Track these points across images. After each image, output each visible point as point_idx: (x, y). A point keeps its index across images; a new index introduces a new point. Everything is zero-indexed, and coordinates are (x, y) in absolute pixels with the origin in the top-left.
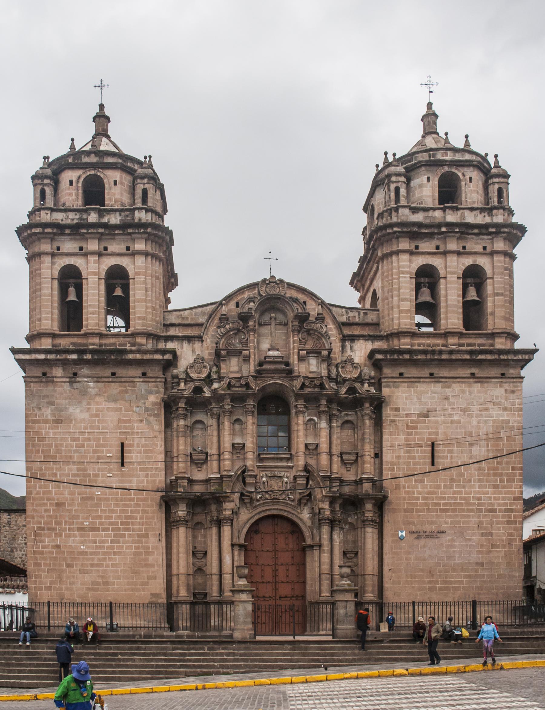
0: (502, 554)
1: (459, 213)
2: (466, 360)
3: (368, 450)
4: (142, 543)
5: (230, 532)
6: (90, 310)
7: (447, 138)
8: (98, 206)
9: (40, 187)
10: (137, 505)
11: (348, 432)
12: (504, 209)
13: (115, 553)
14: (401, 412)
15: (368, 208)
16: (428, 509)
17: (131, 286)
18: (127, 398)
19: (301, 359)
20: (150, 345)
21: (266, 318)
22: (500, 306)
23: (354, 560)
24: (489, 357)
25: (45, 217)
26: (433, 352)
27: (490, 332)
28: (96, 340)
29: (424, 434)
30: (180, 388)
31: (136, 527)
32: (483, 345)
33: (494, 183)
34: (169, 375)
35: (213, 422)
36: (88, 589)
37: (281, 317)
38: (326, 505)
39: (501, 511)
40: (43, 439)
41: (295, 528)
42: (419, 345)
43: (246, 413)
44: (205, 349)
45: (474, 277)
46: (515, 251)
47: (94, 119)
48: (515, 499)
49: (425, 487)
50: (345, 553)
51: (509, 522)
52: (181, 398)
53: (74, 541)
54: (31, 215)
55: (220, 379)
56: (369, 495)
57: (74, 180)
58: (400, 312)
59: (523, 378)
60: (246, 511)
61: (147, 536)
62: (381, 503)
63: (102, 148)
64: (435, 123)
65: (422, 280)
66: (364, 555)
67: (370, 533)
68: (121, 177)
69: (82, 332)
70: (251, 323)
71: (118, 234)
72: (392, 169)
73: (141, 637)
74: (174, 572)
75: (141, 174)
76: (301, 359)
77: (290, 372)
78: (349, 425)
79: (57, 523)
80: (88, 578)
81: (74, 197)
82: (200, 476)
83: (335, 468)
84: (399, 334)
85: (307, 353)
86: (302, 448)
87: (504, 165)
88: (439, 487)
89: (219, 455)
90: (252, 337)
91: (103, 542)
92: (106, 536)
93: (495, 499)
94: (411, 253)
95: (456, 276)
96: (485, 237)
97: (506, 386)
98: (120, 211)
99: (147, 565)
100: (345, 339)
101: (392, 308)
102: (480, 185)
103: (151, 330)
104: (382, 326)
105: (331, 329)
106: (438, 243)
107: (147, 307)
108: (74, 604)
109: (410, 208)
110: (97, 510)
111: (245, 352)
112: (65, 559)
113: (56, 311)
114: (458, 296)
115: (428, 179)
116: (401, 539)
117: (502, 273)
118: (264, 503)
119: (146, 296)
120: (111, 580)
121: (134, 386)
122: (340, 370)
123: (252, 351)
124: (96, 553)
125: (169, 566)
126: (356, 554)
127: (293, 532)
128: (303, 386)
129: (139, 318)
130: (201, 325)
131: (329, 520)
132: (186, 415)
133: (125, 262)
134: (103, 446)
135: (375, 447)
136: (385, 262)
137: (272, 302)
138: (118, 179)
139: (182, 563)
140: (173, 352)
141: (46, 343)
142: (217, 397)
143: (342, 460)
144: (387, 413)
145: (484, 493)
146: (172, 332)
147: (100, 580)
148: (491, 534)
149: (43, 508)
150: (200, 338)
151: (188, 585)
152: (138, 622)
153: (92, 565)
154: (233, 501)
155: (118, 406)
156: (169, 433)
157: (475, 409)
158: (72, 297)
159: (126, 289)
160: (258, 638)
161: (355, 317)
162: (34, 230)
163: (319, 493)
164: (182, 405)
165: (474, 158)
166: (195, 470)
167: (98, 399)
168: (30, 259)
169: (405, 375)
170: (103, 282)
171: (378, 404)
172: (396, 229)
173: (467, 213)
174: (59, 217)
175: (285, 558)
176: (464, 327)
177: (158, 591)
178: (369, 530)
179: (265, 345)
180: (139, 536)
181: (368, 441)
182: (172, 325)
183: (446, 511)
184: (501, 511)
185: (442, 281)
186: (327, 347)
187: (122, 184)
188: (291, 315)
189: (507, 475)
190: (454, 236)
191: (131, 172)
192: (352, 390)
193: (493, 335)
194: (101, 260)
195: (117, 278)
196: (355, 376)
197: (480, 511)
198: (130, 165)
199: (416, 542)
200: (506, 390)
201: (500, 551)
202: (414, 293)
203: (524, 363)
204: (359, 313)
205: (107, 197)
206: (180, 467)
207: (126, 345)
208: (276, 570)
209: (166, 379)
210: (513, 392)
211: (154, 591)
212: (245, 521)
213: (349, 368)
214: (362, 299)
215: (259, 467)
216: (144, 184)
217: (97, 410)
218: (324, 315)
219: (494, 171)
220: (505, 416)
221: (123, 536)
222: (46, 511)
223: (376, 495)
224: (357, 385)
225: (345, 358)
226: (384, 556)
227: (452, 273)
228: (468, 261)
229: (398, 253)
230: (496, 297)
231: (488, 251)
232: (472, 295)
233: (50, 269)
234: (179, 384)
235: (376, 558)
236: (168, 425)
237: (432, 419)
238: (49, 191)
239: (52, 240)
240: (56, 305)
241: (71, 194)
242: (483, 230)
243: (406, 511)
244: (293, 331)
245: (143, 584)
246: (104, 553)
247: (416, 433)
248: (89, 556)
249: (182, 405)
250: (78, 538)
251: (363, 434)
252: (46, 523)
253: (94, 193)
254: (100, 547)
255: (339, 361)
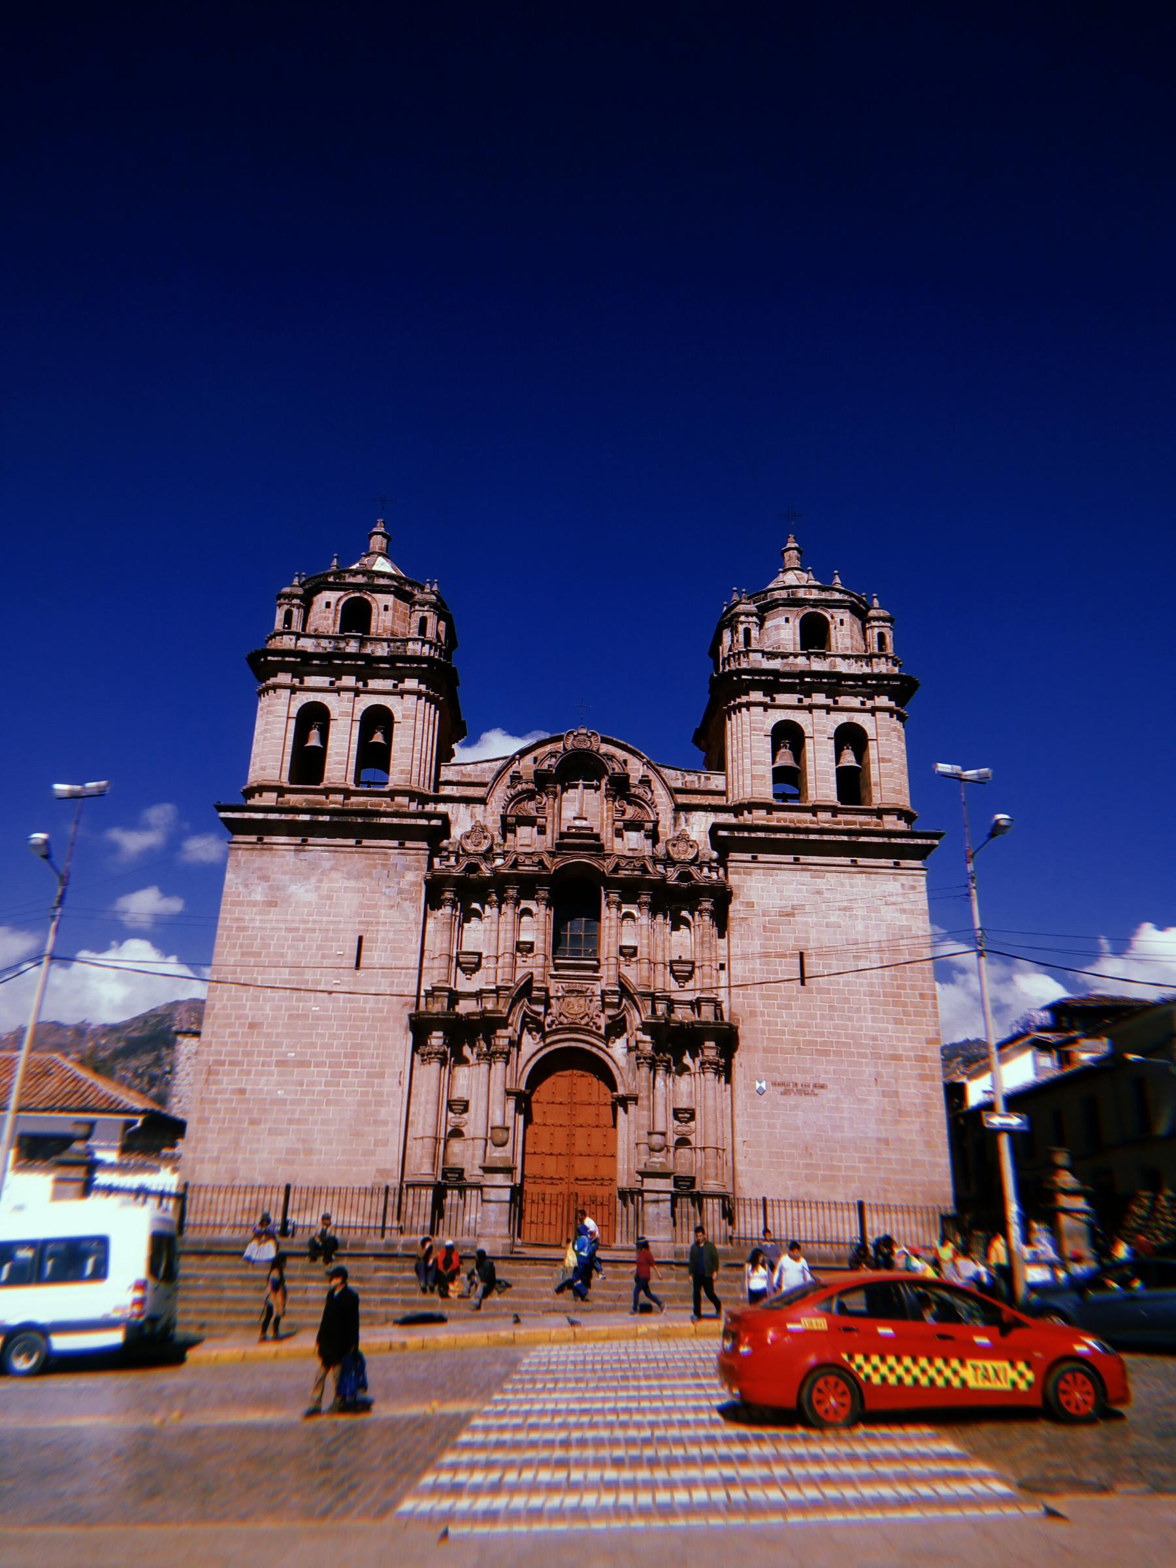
0: (916, 1127)
1: (828, 660)
10: (373, 1027)
13: (329, 1103)
20: (413, 807)
29: (789, 940)
31: (367, 1061)
32: (868, 824)
36: (278, 1161)
40: (245, 929)
44: (490, 816)
48: (929, 1042)
53: (267, 1083)
55: (504, 854)
61: (382, 1075)
63: (375, 568)
76: (619, 834)
77: (601, 848)
79: (246, 1054)
80: (281, 1143)
81: (331, 622)
84: (751, 806)
88: (813, 1017)
91: (313, 1084)
97: (903, 879)
99: (376, 1122)
100: (679, 808)
103: (415, 786)
105: (660, 796)
108: (251, 1188)
109: (764, 653)
115: (787, 620)
116: (761, 1092)
117: (888, 734)
120: (318, 1146)
124: (300, 1102)
128: (617, 868)
130: (484, 785)
134: (333, 940)
138: (390, 604)
140: (444, 817)
145: (880, 1030)
146: (446, 791)
149: (228, 1030)
150: (483, 801)
153: (290, 1121)
155: (360, 885)
158: (314, 741)
159: (388, 737)
163: (635, 1019)
167: (334, 875)
171: (722, 897)
173: (838, 660)
174: (308, 645)
177: (388, 1166)
183: (826, 1053)
189: (914, 1005)
192: (685, 876)
193: (880, 813)
195: (377, 721)
199: (782, 1100)
200: (903, 885)
202: (770, 755)
207: (381, 805)
208: (571, 1136)
215: (552, 977)
217: (330, 890)
220: (903, 920)
221: (345, 1075)
224: (693, 869)
225: (677, 834)
232: (849, 759)
237: (798, 918)
241: (326, 618)
246: (312, 1102)
247: (777, 938)
248: (288, 1107)
252: (230, 1054)
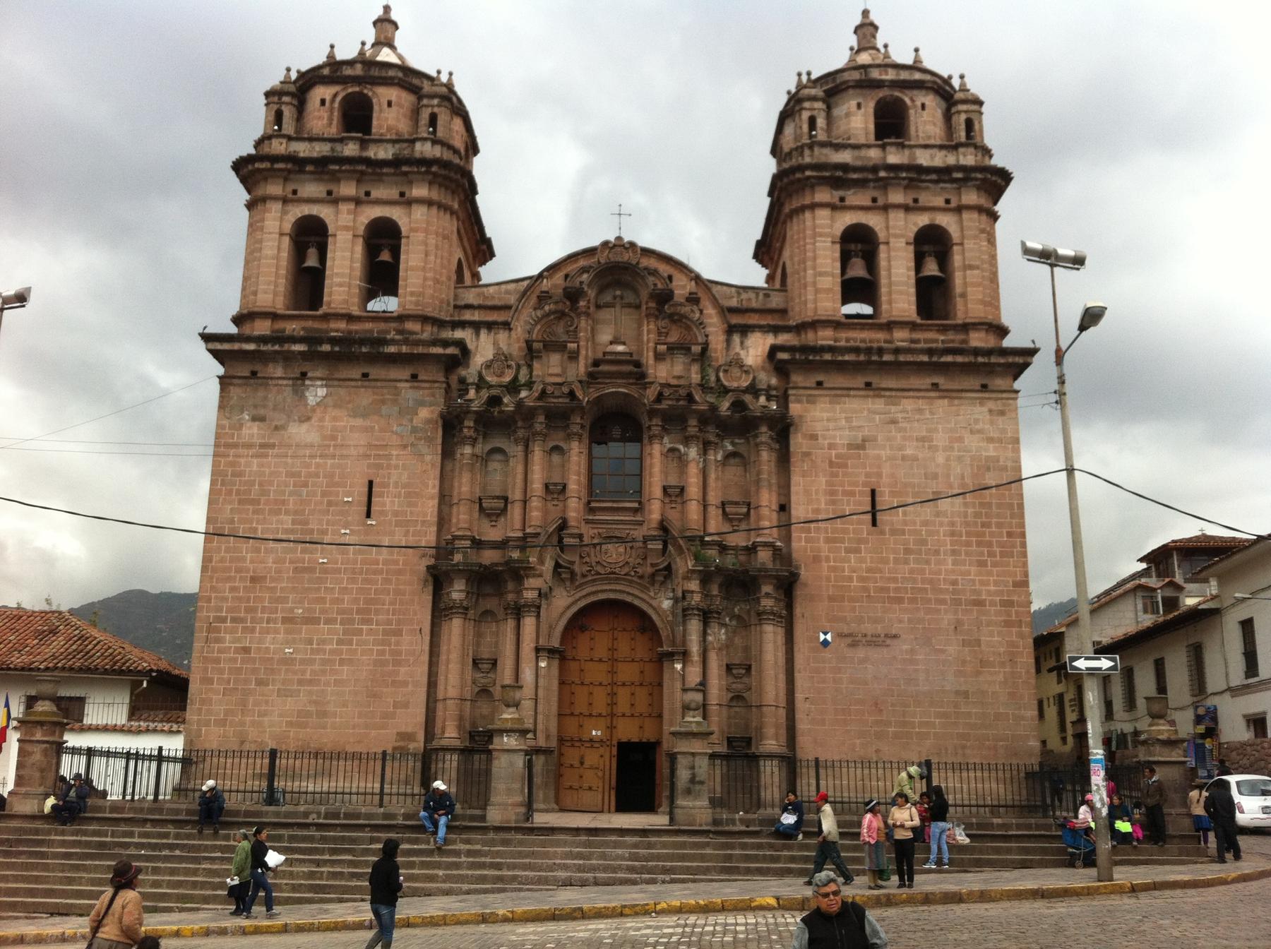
1: (907, 152)
2: (922, 364)
3: (767, 499)
4: (390, 645)
5: (534, 627)
6: (336, 280)
7: (886, 51)
8: (360, 135)
9: (276, 107)
10: (387, 581)
11: (733, 472)
12: (976, 147)
13: (342, 662)
14: (820, 440)
15: (776, 150)
16: (869, 596)
17: (403, 248)
18: (383, 412)
19: (659, 357)
21: (607, 298)
22: (974, 285)
23: (745, 680)
24: (959, 359)
25: (278, 147)
26: (869, 351)
27: (960, 322)
28: (342, 325)
30: (467, 397)
33: (959, 112)
34: (454, 379)
35: (518, 450)
36: (290, 724)
37: (630, 297)
38: (694, 585)
39: (993, 603)
40: (240, 474)
41: (644, 623)
42: (848, 340)
43: (569, 437)
44: (511, 342)
45: (932, 244)
46: (996, 208)
47: (375, 23)
49: (862, 560)
50: (729, 668)
51: (1008, 624)
52: (469, 412)
53: (274, 641)
54: (259, 143)
55: (529, 385)
56: (766, 570)
57: (328, 98)
58: (817, 291)
59: (1017, 392)
60: (565, 593)
61: (398, 633)
62: (788, 585)
64: (874, 37)
65: (853, 247)
66: (760, 672)
67: (771, 635)
68: (399, 97)
69: (320, 312)
70: (582, 303)
71: (387, 174)
72: (806, 92)
73: (319, 818)
74: (440, 695)
75: (438, 100)
76: (659, 357)
77: (643, 376)
78: (737, 460)
79: (248, 610)
80: (290, 704)
81: (325, 121)
82: (493, 533)
83: (712, 528)
84: (814, 325)
85: (668, 349)
86: (658, 492)
87: (975, 88)
89: (525, 502)
90: (583, 324)
91: (323, 642)
92: (330, 632)
93: (982, 583)
94: (833, 207)
95: (903, 240)
96: (948, 185)
97: (991, 405)
98: (394, 142)
100: (731, 330)
101: (805, 286)
102: (939, 114)
103: (429, 311)
104: (791, 313)
105: (710, 316)
106: (875, 194)
107: (425, 279)
110: (319, 589)
111: (572, 346)
112: (254, 671)
113: (282, 281)
114: (908, 269)
115: (859, 106)
117: (975, 237)
118: (594, 580)
119: (426, 263)
120: (331, 708)
121: (398, 395)
122: (721, 374)
123: (582, 343)
125: (432, 684)
126: (749, 668)
127: (643, 630)
128: (660, 398)
129: (412, 294)
130: (508, 307)
131: (698, 609)
132: (476, 439)
133: (395, 213)
134: (337, 485)
135: (779, 494)
136: (795, 220)
137: (618, 274)
138: (394, 99)
139: (454, 680)
140: (461, 344)
141: (262, 328)
142: (525, 414)
143: (725, 514)
144: (798, 442)
145: (962, 574)
146: (468, 316)
147: (312, 708)
148: (978, 642)
150: (506, 325)
151: (461, 718)
152: (341, 784)
153: (300, 682)
154: (540, 576)
156: (449, 466)
157: (940, 439)
160: (540, 819)
161: (750, 299)
162: (257, 165)
164: (469, 423)
165: (928, 77)
166: (486, 524)
168: (250, 206)
169: (825, 385)
170: (360, 241)
171: (783, 428)
172: (808, 173)
175: (628, 672)
176: (918, 314)
178: (769, 629)
179: (605, 337)
180: (385, 633)
181: (765, 483)
182: (469, 307)
183: (900, 600)
184: (993, 603)
185: (882, 248)
186: (700, 340)
187: (400, 105)
188: (644, 294)
189: (1000, 544)
190: (899, 185)
191: (415, 91)
192: (738, 405)
193: (966, 327)
194: (359, 209)
196: (745, 384)
197: (957, 602)
198: (416, 81)
199: (849, 653)
200: (990, 411)
201: (996, 673)
202: (838, 265)
203: (1018, 370)
204: (757, 294)
205: (375, 122)
206: (463, 518)
209: (448, 384)
210: (1002, 413)
211: (403, 729)
212: (561, 610)
213: (736, 372)
214: (770, 279)
216: (433, 106)
217: (334, 429)
218: (700, 295)
219: (959, 96)
221: (360, 632)
222: (233, 589)
223: (777, 570)
224: (748, 398)
226: (797, 675)
227: (896, 236)
228: (923, 220)
229: (813, 206)
230: (968, 272)
231: (953, 205)
232: (931, 268)
233: (279, 220)
234: (467, 391)
235: (782, 677)
236: (447, 453)
237: (871, 452)
238: (288, 112)
239: (286, 180)
240: (283, 272)
242: (943, 174)
243: (832, 599)
244: (647, 316)
245: (385, 716)
247: (845, 475)
249: (469, 423)
250: (281, 636)
251: (759, 473)
252: (229, 610)
253: (357, 116)
254: (318, 651)
255: (721, 361)
